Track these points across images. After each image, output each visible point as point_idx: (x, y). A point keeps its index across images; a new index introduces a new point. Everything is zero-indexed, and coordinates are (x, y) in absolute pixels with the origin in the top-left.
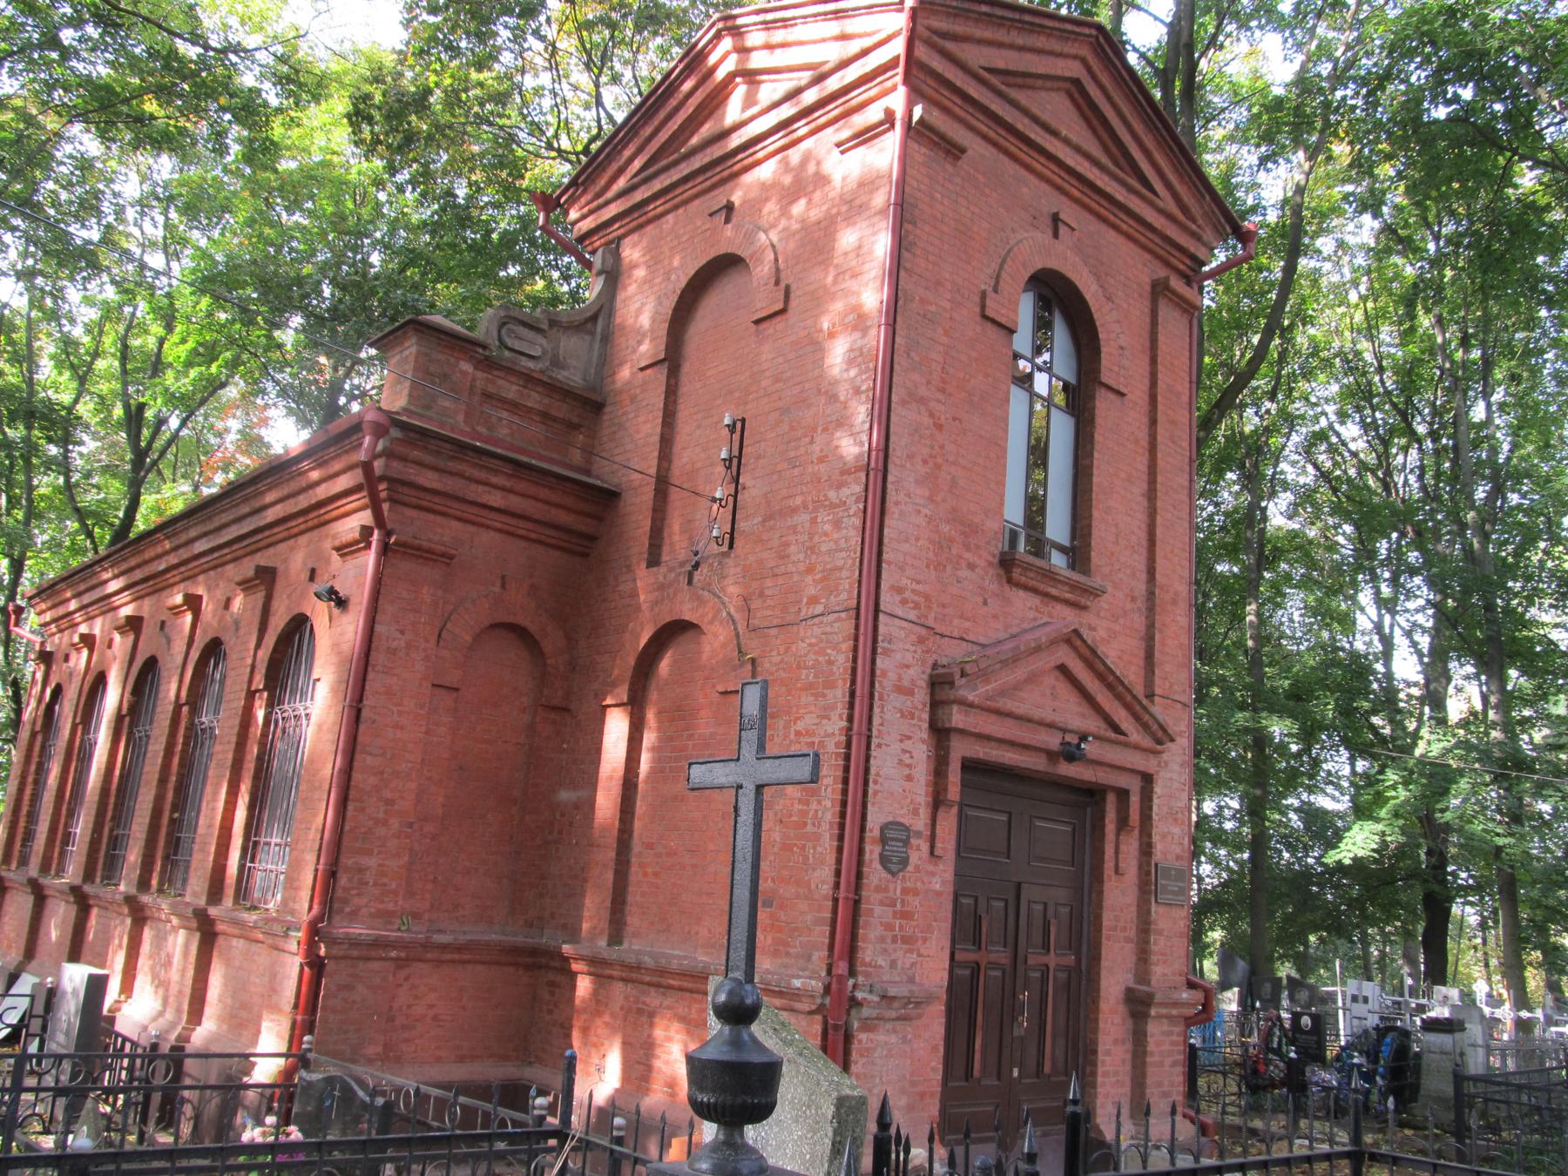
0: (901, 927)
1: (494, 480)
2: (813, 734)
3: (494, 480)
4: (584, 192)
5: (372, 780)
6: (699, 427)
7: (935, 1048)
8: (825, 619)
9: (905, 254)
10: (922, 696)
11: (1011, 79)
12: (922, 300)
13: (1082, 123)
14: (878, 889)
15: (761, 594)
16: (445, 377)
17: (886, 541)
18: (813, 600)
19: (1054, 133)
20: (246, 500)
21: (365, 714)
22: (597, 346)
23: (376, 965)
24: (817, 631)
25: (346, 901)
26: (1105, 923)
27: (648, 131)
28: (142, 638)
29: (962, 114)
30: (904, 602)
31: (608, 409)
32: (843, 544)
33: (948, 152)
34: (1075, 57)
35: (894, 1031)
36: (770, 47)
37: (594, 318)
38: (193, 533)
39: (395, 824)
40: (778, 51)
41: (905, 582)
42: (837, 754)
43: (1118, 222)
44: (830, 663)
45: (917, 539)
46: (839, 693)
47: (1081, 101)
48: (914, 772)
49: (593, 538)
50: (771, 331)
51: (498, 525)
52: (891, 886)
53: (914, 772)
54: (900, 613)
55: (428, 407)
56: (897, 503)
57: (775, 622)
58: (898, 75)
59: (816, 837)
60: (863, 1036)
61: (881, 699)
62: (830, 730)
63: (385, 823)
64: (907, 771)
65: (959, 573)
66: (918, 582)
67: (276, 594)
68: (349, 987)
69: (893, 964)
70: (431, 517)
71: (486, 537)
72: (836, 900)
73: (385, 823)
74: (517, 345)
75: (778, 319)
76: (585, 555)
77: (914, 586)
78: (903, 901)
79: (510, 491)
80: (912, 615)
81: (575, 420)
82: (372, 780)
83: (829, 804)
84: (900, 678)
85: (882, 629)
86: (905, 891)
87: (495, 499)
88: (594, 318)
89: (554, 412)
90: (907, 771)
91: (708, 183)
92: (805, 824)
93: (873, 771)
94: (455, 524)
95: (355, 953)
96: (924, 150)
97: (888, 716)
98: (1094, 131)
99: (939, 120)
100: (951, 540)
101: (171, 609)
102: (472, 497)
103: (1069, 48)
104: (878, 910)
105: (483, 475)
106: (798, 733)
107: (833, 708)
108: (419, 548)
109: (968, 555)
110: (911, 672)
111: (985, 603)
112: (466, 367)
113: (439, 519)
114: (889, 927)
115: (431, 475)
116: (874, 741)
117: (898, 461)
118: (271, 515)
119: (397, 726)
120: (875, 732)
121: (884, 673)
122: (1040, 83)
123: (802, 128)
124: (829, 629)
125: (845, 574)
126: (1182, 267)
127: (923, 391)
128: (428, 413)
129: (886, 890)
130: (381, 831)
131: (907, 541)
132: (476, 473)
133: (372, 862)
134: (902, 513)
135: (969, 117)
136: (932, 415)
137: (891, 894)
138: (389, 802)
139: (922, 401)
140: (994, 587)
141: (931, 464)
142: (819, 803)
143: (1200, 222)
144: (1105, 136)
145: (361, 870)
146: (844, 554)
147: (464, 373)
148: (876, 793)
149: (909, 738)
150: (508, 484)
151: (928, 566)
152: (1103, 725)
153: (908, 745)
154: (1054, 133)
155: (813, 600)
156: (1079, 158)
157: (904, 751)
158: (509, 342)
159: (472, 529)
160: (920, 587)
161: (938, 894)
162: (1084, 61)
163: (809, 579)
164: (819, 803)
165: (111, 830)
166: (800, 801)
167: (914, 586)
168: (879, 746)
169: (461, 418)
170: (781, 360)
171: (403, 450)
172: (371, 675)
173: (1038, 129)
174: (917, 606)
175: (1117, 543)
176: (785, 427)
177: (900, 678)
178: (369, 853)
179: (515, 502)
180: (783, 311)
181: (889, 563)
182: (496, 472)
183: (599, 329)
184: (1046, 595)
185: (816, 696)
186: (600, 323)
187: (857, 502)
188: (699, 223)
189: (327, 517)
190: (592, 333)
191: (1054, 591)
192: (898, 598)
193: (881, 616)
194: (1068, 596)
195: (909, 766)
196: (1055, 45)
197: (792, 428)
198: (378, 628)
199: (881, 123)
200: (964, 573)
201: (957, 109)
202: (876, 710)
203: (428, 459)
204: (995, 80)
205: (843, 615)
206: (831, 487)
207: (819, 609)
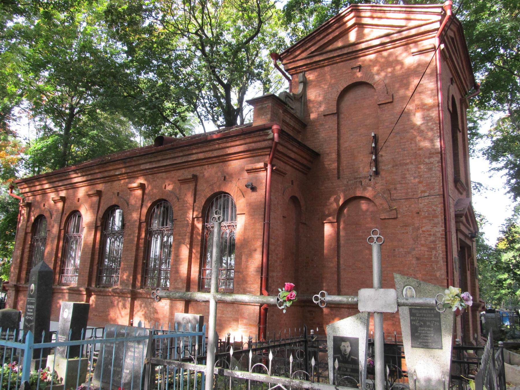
2: (430, 231)
4: (291, 55)
6: (352, 135)
8: (430, 197)
15: (395, 189)
18: (424, 192)
20: (182, 151)
22: (303, 106)
24: (426, 201)
27: (318, 38)
28: (103, 198)
31: (308, 127)
32: (434, 175)
36: (372, 17)
37: (301, 97)
38: (141, 162)
39: (278, 261)
40: (376, 19)
42: (442, 238)
44: (434, 210)
46: (440, 219)
49: (309, 169)
50: (386, 108)
51: (291, 164)
57: (403, 198)
58: (436, 34)
59: (437, 262)
62: (438, 230)
67: (198, 184)
72: (448, 280)
75: (389, 104)
76: (306, 174)
81: (300, 130)
83: (441, 252)
87: (292, 155)
88: (301, 97)
89: (296, 127)
91: (349, 58)
92: (431, 258)
101: (129, 188)
106: (423, 231)
107: (438, 223)
118: (194, 157)
123: (389, 46)
124: (432, 200)
125: (436, 184)
142: (437, 252)
146: (435, 178)
155: (424, 192)
163: (420, 185)
164: (437, 252)
165: (98, 268)
166: (428, 251)
170: (392, 117)
172: (271, 213)
176: (398, 138)
179: (298, 158)
180: (392, 102)
183: (303, 101)
185: (430, 220)
186: (303, 98)
187: (438, 162)
188: (344, 70)
189: (227, 159)
190: (301, 102)
197: (401, 139)
199: (432, 48)
205: (438, 196)
206: (425, 158)
207: (427, 194)
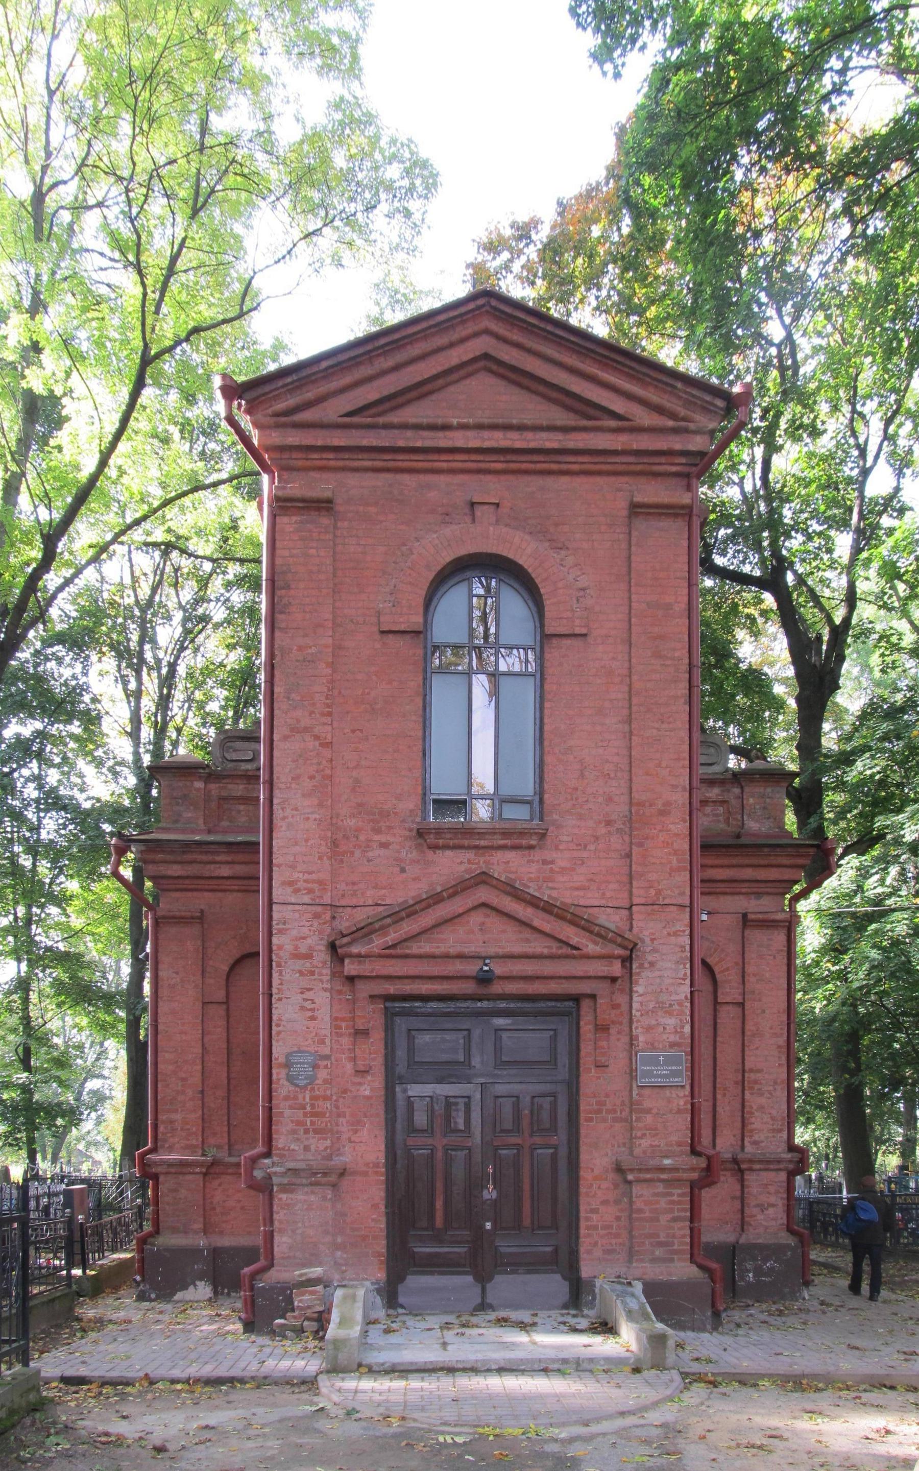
0: (312, 1123)
1: (218, 858)
3: (218, 858)
5: (171, 1067)
7: (375, 1206)
9: (279, 616)
10: (322, 956)
11: (373, 411)
12: (300, 649)
13: (516, 390)
14: (286, 1098)
16: (185, 797)
17: (275, 850)
19: (446, 427)
21: (160, 1027)
23: (190, 1177)
25: (165, 1141)
26: (582, 1107)
29: (340, 463)
30: (297, 891)
33: (318, 509)
34: (476, 335)
35: (313, 1192)
39: (190, 1092)
41: (296, 875)
43: (564, 467)
45: (307, 840)
47: (501, 370)
48: (316, 1013)
52: (300, 1096)
53: (316, 1013)
54: (293, 900)
55: (176, 821)
56: (284, 818)
60: (284, 1196)
61: (279, 965)
63: (183, 1092)
64: (310, 1014)
65: (370, 854)
66: (310, 873)
68: (176, 1190)
69: (307, 1148)
70: (189, 894)
71: (230, 898)
73: (183, 1092)
74: (235, 756)
77: (306, 876)
78: (313, 1106)
79: (232, 863)
80: (306, 899)
82: (171, 1067)
84: (296, 948)
85: (275, 916)
86: (312, 1098)
87: (225, 871)
90: (310, 1014)
93: (275, 1018)
94: (206, 894)
95: (173, 1170)
96: (294, 519)
97: (287, 977)
98: (528, 389)
99: (297, 487)
100: (358, 830)
102: (207, 874)
103: (471, 328)
104: (287, 1112)
105: (210, 858)
108: (174, 917)
109: (377, 838)
110: (309, 941)
111: (403, 870)
112: (199, 785)
113: (195, 894)
114: (299, 1123)
115: (175, 867)
116: (275, 997)
117: (283, 786)
119: (181, 1033)
120: (274, 991)
121: (280, 947)
122: (441, 382)
126: (674, 469)
127: (306, 722)
128: (178, 825)
129: (295, 1098)
130: (181, 1098)
131: (296, 844)
132: (204, 858)
133: (178, 1117)
134: (289, 826)
135: (348, 463)
136: (317, 738)
137: (300, 1100)
138: (183, 1080)
139: (306, 730)
140: (414, 855)
141: (318, 777)
143: (683, 412)
144: (541, 388)
145: (172, 1122)
147: (198, 790)
148: (279, 1033)
149: (309, 990)
150: (229, 859)
151: (320, 858)
152: (555, 945)
153: (308, 995)
154: (446, 427)
156: (486, 434)
157: (305, 1000)
158: (228, 756)
159: (219, 894)
160: (314, 876)
161: (368, 1098)
162: (487, 331)
167: (306, 876)
168: (280, 999)
169: (201, 821)
171: (150, 857)
172: (160, 1004)
173: (426, 434)
174: (310, 891)
175: (582, 776)
177: (296, 948)
178: (176, 1111)
181: (279, 866)
182: (218, 853)
184: (476, 847)
191: (483, 843)
192: (289, 890)
193: (275, 907)
194: (502, 842)
195: (313, 1010)
196: (443, 340)
198: (160, 973)
200: (376, 852)
201: (332, 463)
202: (275, 975)
203: (169, 857)
204: (355, 420)
